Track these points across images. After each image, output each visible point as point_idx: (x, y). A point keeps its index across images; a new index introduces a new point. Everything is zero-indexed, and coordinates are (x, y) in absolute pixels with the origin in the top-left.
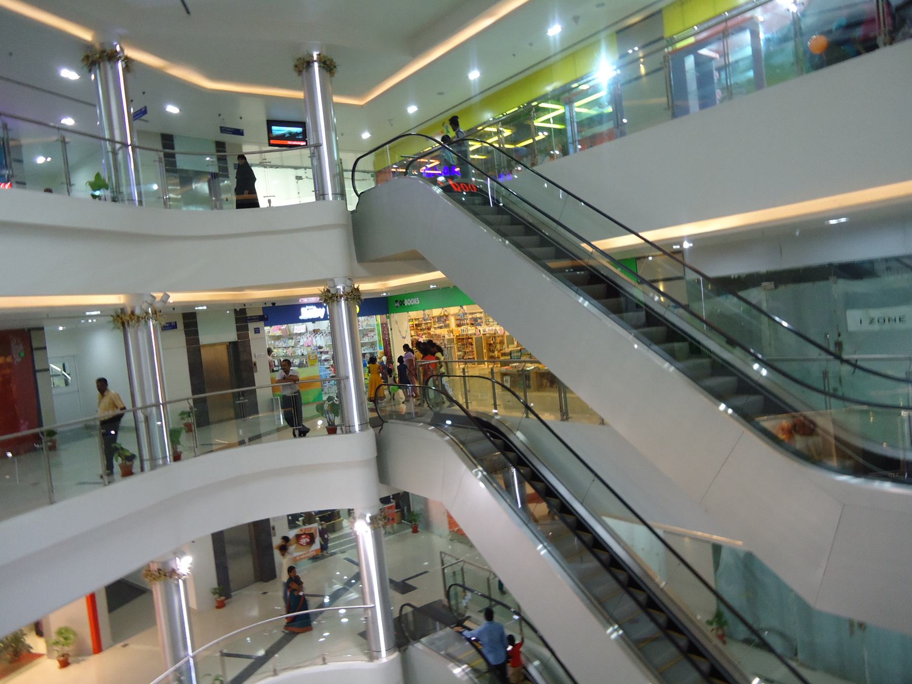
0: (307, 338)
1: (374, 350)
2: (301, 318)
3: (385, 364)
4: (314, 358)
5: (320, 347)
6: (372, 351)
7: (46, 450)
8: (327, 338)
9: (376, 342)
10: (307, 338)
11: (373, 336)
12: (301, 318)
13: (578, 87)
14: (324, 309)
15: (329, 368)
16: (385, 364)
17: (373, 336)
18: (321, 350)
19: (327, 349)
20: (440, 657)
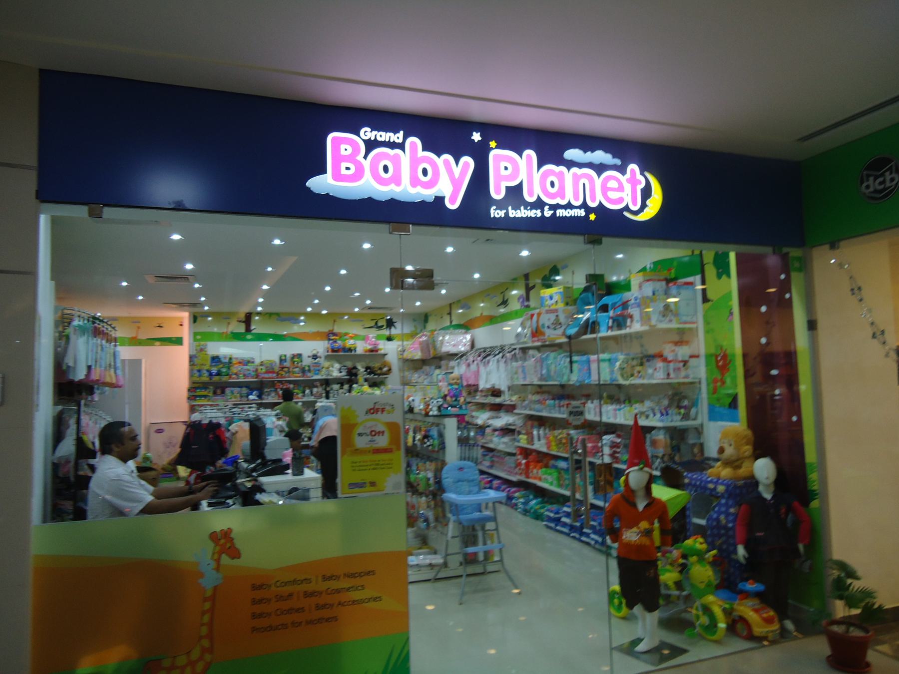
0: (469, 365)
1: (686, 417)
2: (320, 184)
3: (768, 496)
4: (383, 441)
5: (496, 393)
6: (675, 421)
7: (734, 355)
8: (514, 364)
9: (694, 385)
10: (469, 365)
11: (685, 363)
12: (320, 184)
13: (348, 589)
14: (468, 161)
15: (514, 455)
16: (768, 496)
17: (685, 363)
18: (498, 400)
19: (514, 398)
20: (586, 550)
